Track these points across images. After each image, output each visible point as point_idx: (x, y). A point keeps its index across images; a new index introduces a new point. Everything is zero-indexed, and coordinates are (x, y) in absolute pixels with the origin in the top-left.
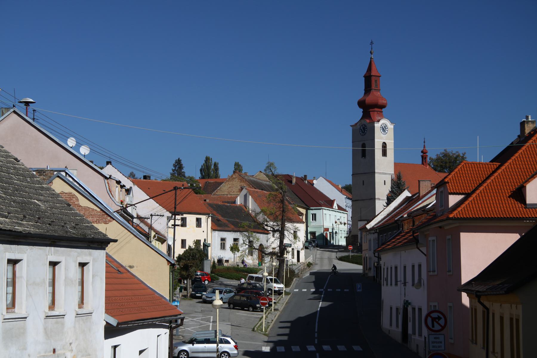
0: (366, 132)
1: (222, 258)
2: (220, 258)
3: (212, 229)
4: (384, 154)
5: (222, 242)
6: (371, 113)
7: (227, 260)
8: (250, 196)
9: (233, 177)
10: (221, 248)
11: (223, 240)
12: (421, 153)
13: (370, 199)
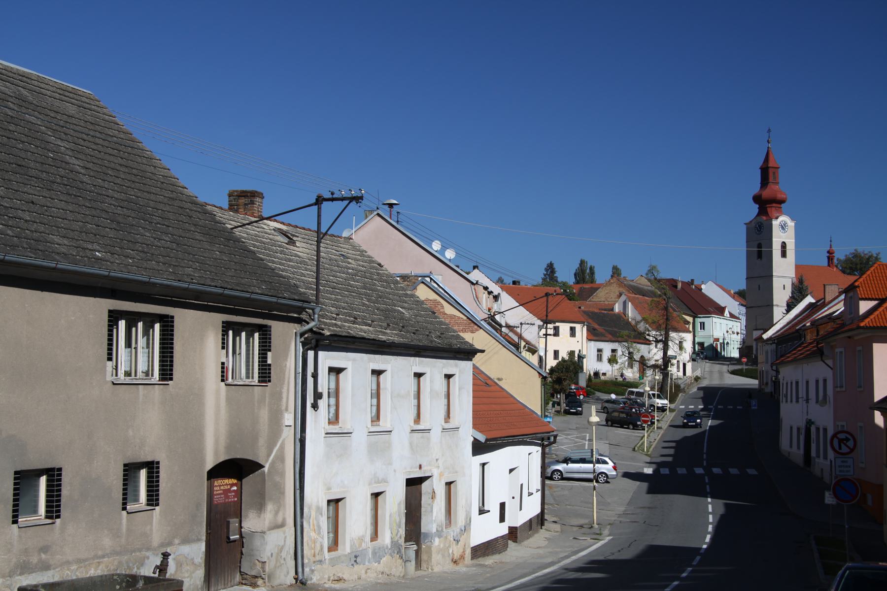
0: (762, 230)
3: (587, 339)
5: (599, 353)
6: (769, 209)
10: (598, 360)
11: (600, 351)
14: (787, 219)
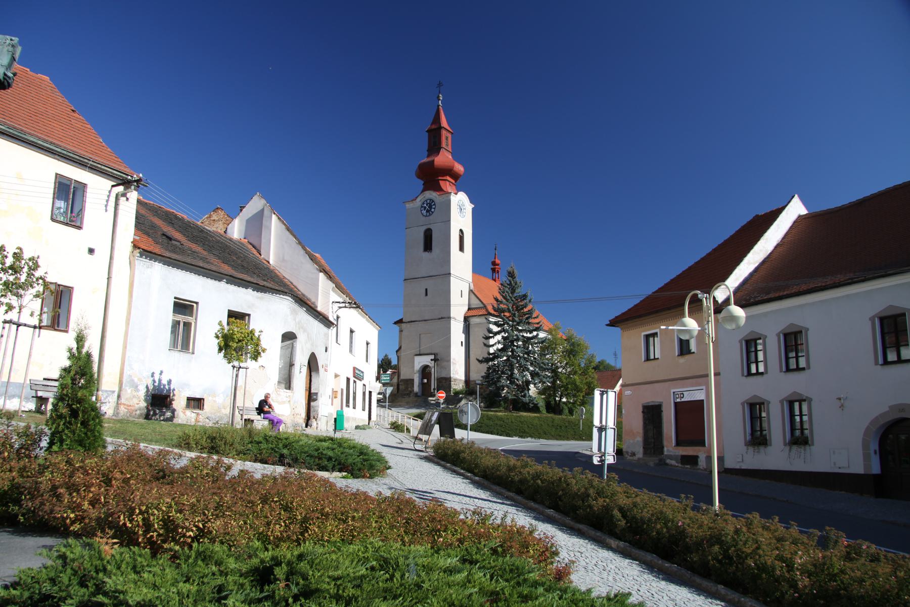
0: (433, 210)
1: (170, 382)
2: (160, 381)
3: (135, 246)
4: (461, 248)
5: (181, 318)
6: (442, 183)
7: (198, 396)
8: (274, 216)
9: (212, 219)
10: (174, 345)
11: (183, 307)
12: (491, 264)
13: (439, 319)
14: (466, 200)
